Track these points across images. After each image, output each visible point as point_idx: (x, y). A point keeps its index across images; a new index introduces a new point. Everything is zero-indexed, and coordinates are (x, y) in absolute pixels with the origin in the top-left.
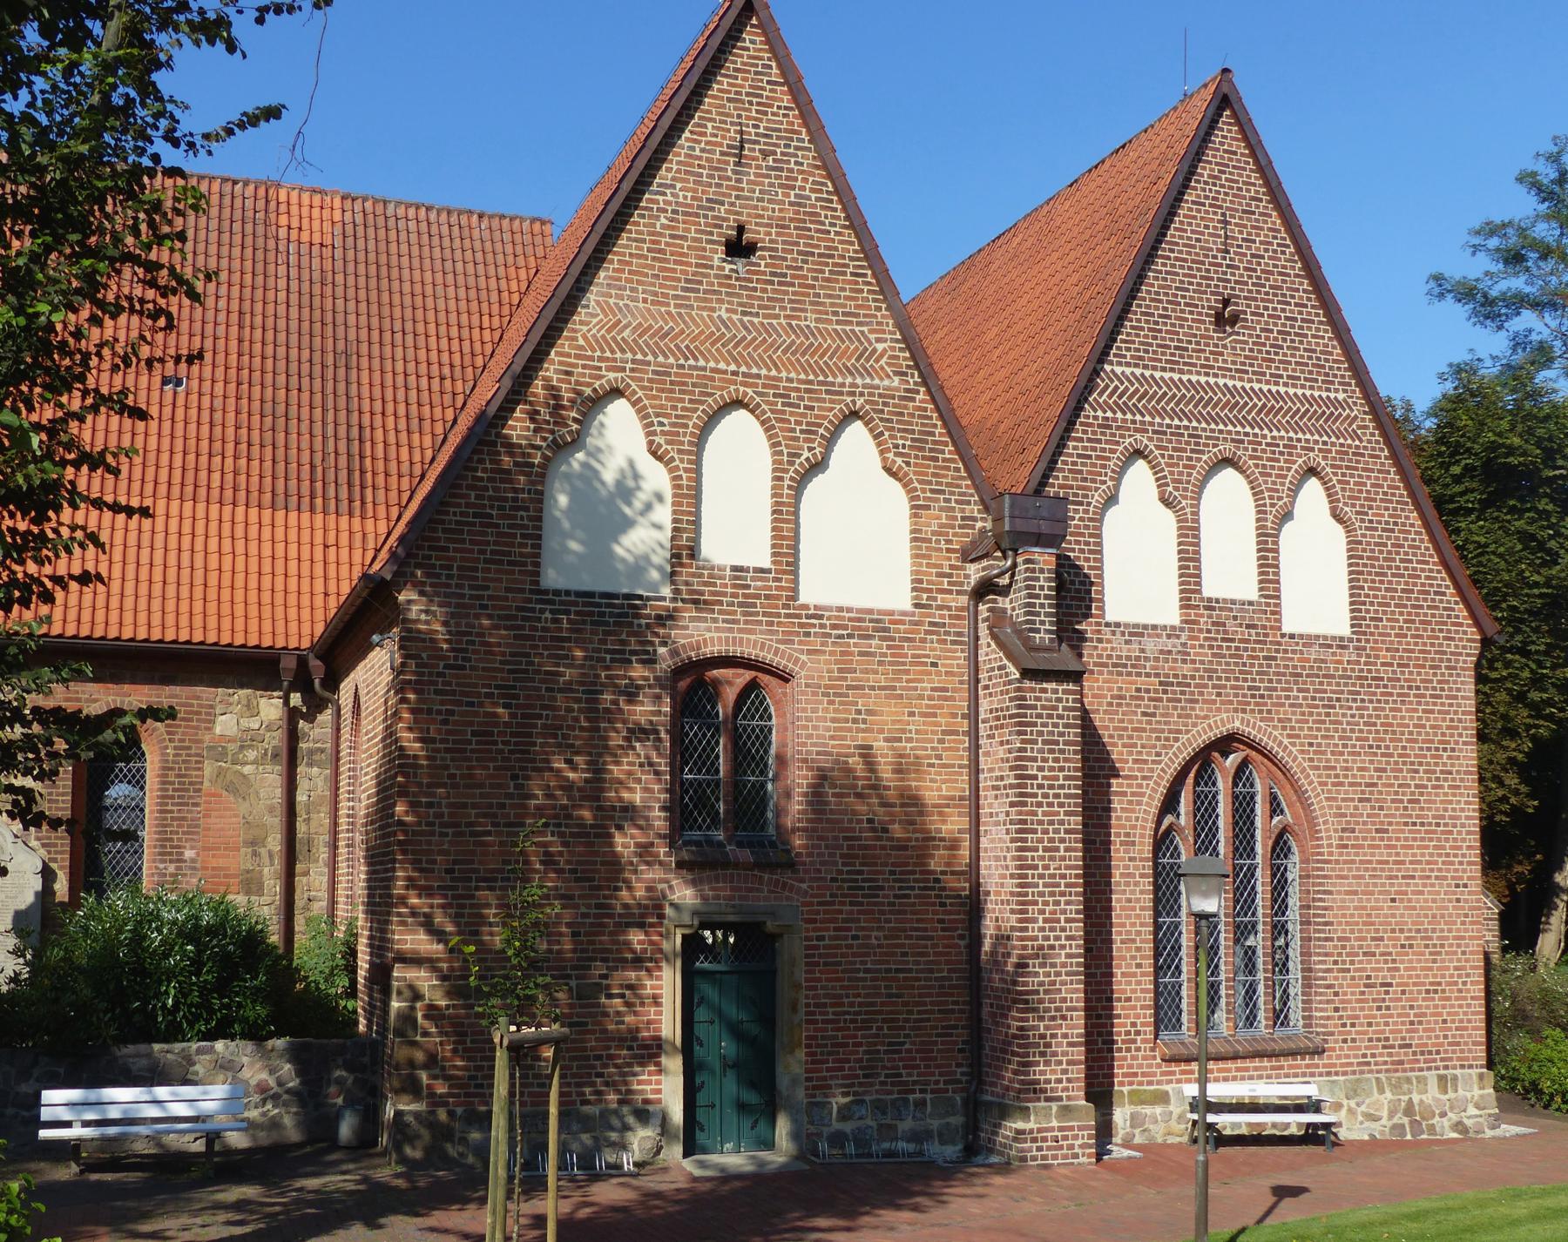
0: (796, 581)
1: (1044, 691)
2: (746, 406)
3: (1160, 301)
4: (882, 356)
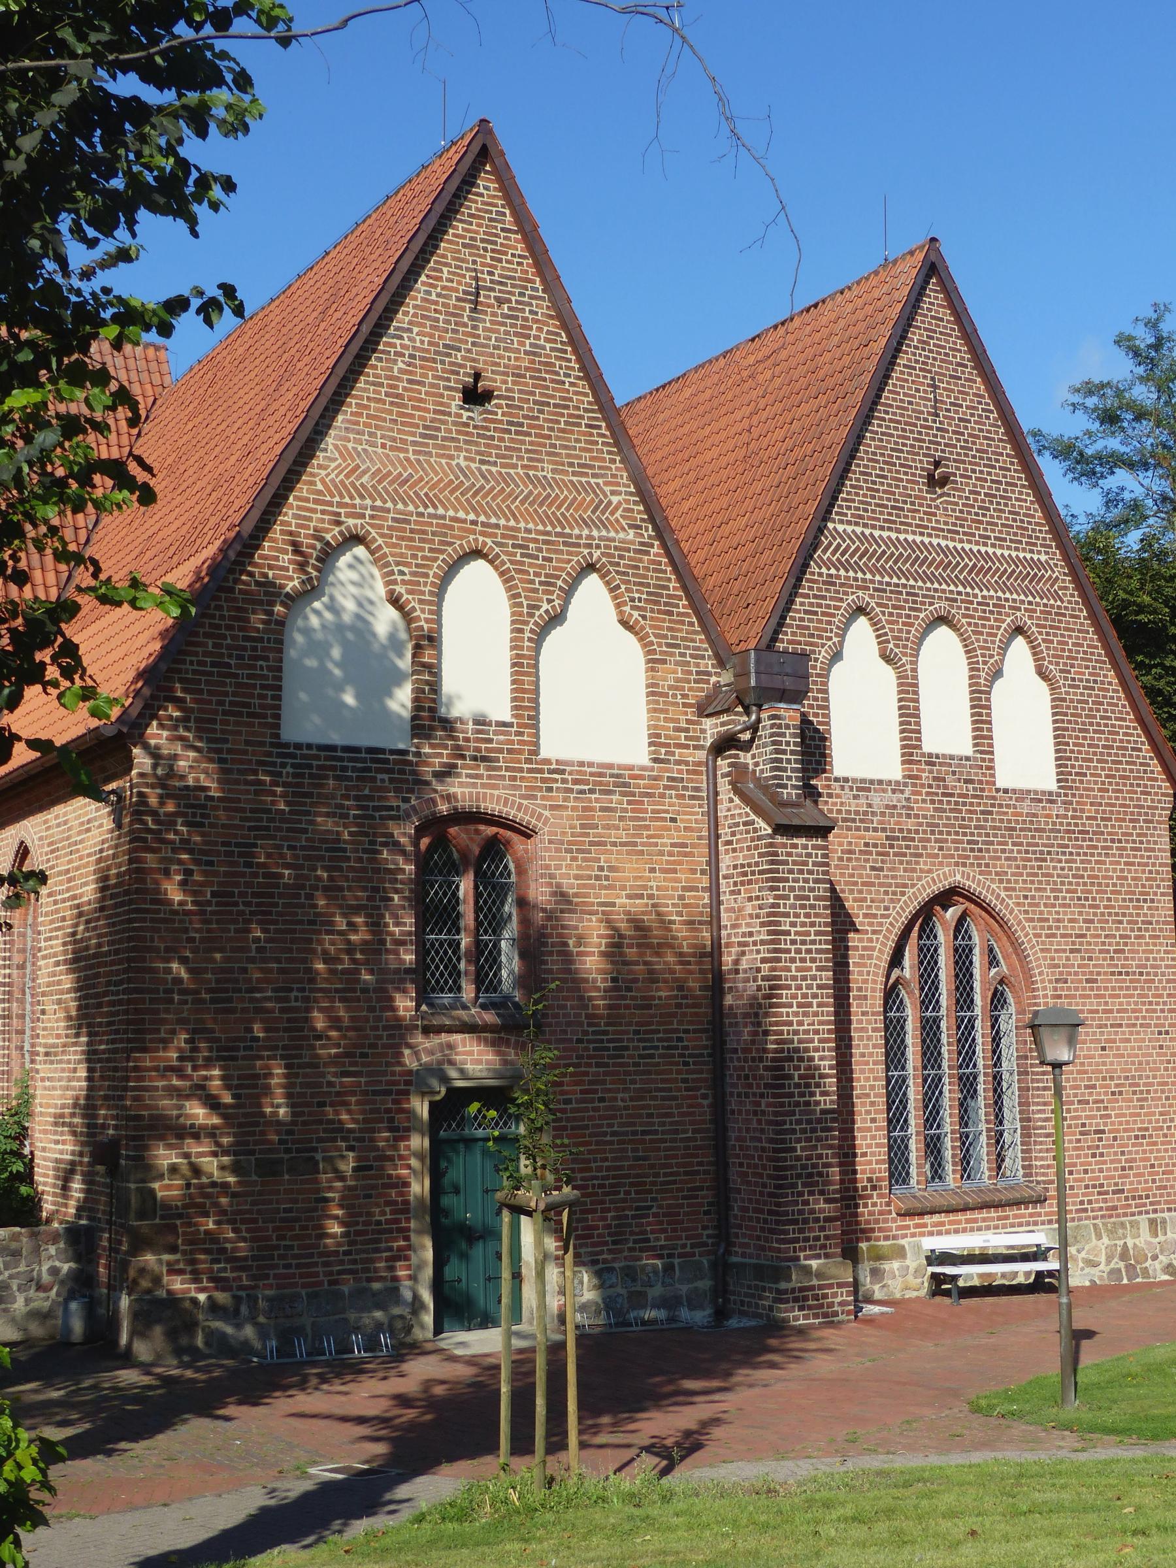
1: (795, 846)
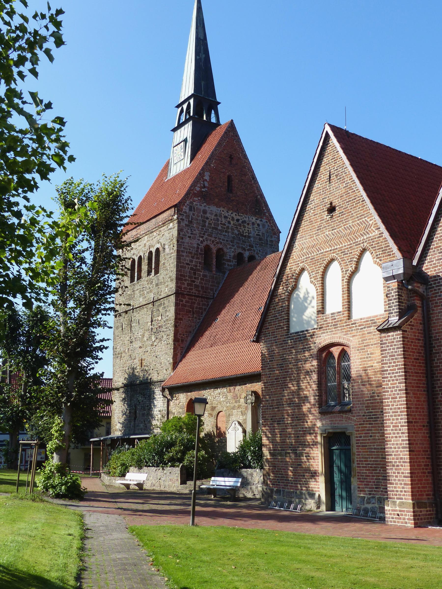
1: (389, 336)
4: (372, 225)
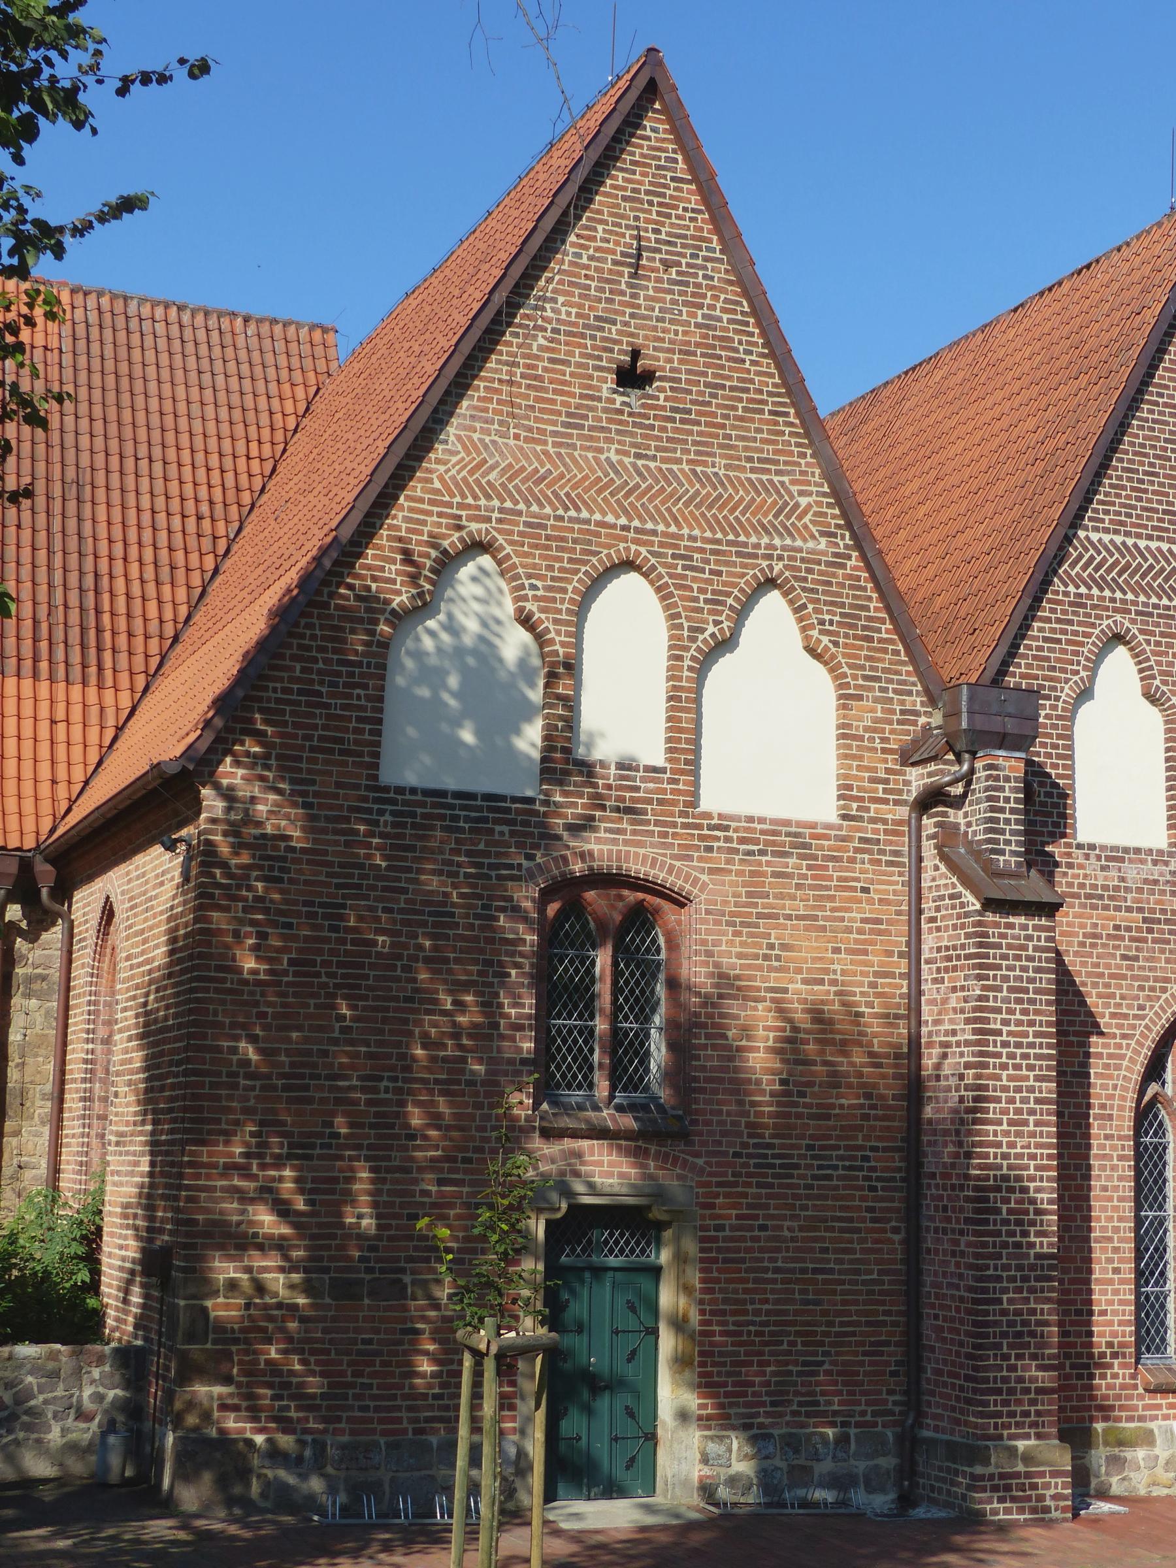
0: (696, 784)
1: (1011, 926)
2: (638, 569)
3: (1146, 455)
